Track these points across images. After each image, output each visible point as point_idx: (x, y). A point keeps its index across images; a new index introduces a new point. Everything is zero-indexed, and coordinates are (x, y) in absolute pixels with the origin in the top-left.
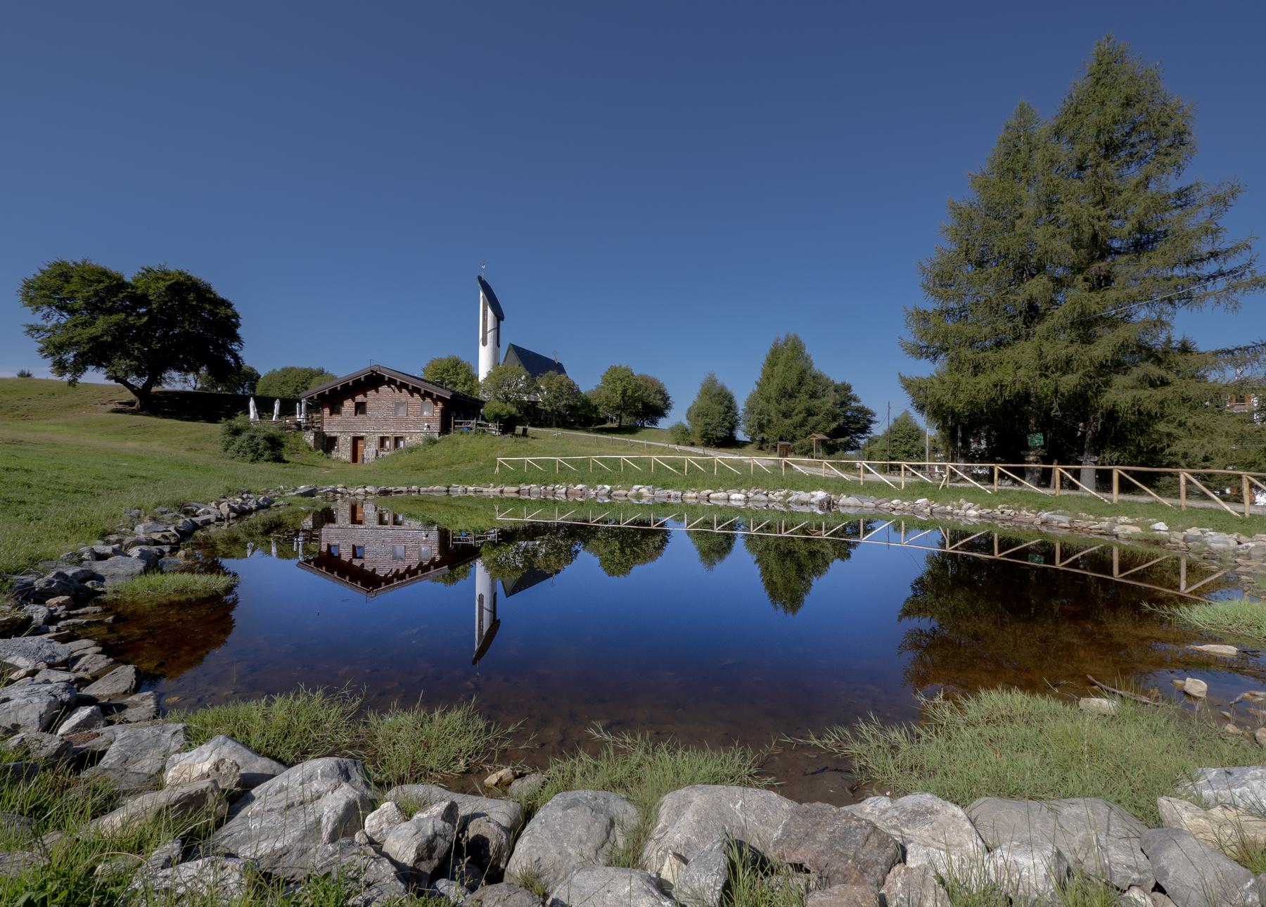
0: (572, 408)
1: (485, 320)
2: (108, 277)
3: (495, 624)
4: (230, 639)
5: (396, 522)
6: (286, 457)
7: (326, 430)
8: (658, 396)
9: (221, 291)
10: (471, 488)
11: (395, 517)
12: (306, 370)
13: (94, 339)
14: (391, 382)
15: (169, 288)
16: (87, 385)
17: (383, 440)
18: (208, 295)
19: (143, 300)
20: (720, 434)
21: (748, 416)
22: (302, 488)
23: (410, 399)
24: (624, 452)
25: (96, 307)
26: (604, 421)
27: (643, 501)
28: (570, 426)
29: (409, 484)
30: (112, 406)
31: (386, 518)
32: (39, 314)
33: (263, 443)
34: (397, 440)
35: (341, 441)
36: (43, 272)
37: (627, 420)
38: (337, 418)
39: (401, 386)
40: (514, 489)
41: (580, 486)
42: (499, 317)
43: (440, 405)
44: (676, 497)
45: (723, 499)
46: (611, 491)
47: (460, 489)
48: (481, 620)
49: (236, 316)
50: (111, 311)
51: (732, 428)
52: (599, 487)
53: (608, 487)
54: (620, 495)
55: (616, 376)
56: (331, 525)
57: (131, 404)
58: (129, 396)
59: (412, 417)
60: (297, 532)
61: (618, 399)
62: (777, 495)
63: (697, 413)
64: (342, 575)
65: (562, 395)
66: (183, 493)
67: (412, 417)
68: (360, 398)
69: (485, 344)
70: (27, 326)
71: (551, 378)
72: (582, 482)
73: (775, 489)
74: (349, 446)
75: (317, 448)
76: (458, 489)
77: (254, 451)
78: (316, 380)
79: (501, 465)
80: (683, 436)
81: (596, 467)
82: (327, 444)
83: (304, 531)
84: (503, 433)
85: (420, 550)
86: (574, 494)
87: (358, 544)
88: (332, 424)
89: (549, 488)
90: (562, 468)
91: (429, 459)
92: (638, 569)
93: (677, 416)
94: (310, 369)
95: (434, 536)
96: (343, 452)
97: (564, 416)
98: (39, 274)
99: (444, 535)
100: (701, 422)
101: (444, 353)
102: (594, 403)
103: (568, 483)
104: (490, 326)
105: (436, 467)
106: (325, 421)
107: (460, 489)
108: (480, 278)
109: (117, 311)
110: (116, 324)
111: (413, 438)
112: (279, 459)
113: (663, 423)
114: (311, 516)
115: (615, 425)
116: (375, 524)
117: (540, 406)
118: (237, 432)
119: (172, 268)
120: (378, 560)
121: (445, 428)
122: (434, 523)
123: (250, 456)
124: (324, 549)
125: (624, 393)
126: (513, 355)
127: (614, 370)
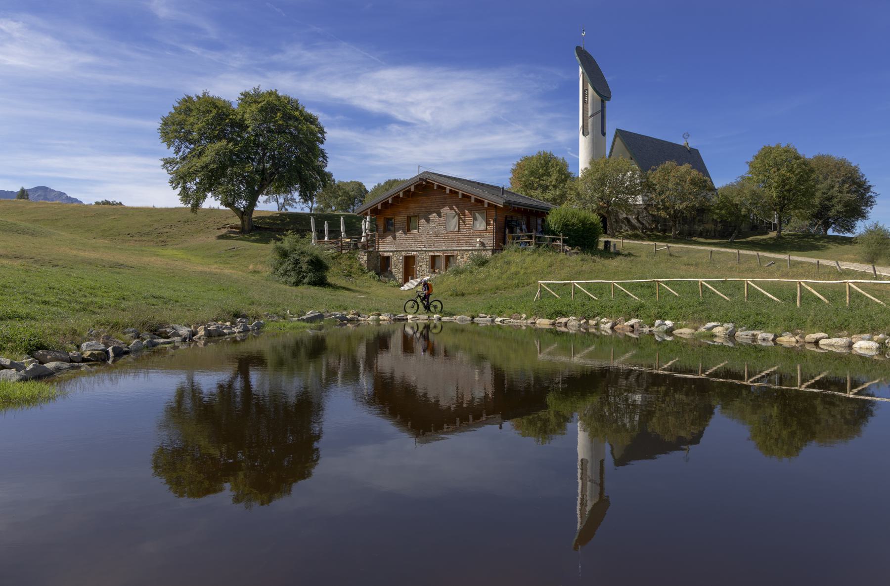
6: (330, 280)
15: (261, 110)
16: (212, 210)
17: (433, 258)
24: (751, 271)
28: (685, 237)
30: (223, 232)
35: (393, 261)
36: (175, 108)
41: (633, 321)
42: (604, 94)
52: (658, 322)
53: (669, 323)
55: (770, 161)
58: (237, 221)
70: (164, 160)
76: (484, 320)
89: (592, 322)
92: (812, 450)
95: (489, 376)
98: (173, 111)
99: (499, 376)
102: (736, 200)
112: (321, 282)
113: (860, 227)
121: (500, 244)
127: (767, 152)
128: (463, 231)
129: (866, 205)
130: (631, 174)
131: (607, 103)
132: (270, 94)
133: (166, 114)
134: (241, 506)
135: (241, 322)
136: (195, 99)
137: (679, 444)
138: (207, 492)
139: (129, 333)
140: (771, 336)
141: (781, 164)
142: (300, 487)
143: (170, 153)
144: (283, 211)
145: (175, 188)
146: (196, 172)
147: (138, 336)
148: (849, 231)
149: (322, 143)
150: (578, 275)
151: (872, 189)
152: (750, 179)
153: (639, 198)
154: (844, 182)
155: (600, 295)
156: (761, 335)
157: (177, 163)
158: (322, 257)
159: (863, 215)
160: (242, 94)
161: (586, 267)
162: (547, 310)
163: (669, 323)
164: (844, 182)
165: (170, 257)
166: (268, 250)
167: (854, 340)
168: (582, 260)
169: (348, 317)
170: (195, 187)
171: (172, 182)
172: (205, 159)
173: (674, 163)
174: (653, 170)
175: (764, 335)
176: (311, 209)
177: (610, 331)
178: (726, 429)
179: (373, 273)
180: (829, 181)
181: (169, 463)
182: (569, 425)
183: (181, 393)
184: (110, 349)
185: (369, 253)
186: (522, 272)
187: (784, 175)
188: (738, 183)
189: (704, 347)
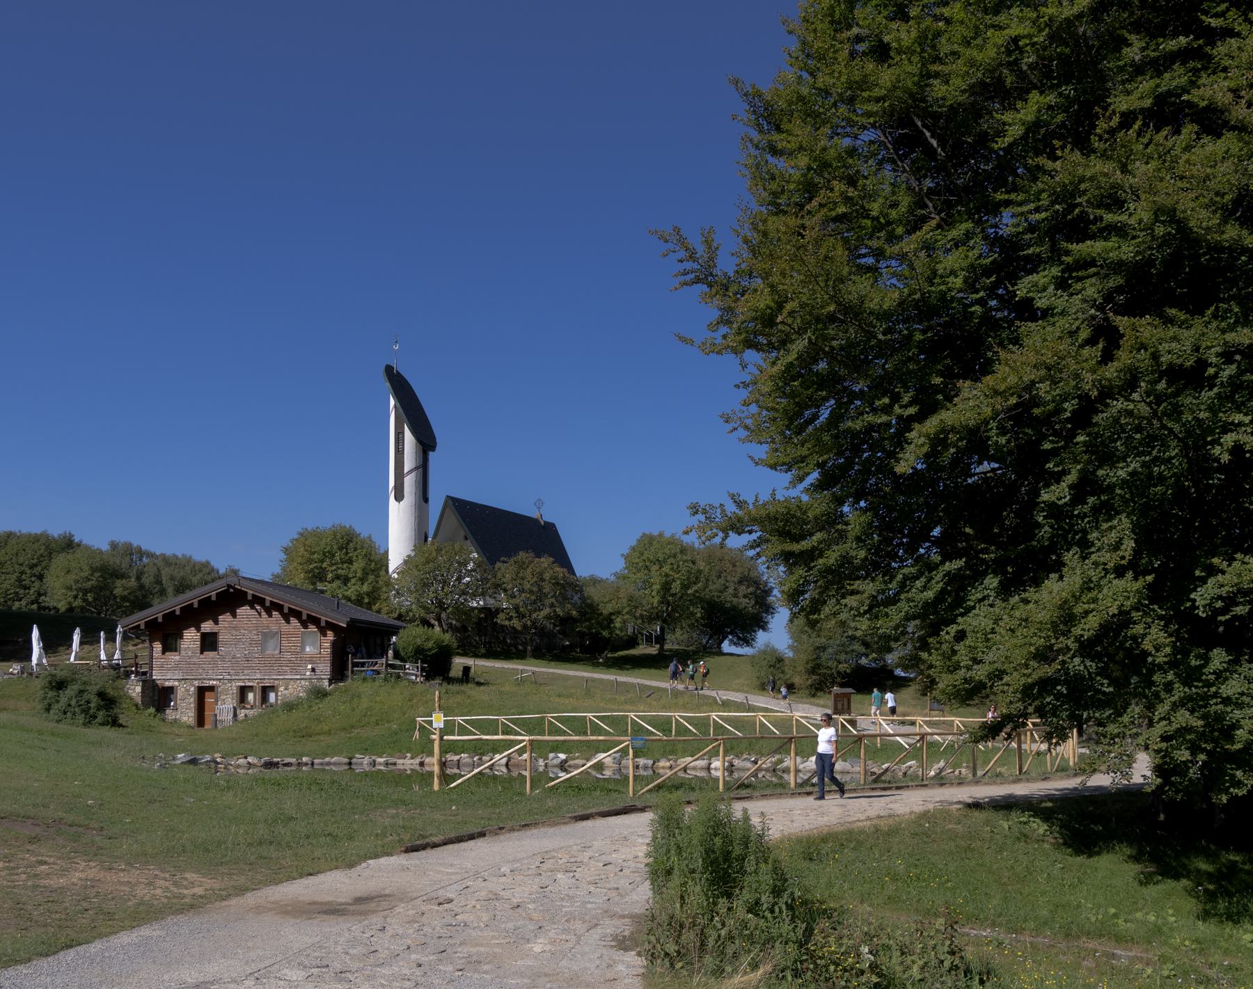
7: (156, 676)
8: (743, 589)
10: (381, 760)
12: (35, 539)
14: (257, 601)
17: (243, 691)
24: (676, 708)
26: (632, 642)
27: (608, 773)
33: (95, 702)
34: (265, 691)
35: (180, 693)
38: (173, 657)
42: (426, 443)
43: (331, 636)
44: (645, 768)
45: (702, 769)
46: (565, 761)
47: (366, 760)
52: (551, 755)
53: (562, 756)
59: (288, 656)
65: (541, 596)
67: (288, 656)
68: (207, 626)
69: (399, 498)
71: (522, 566)
74: (192, 701)
75: (146, 705)
77: (85, 711)
78: (60, 560)
84: (428, 678)
88: (168, 668)
91: (318, 720)
94: (45, 535)
101: (326, 517)
104: (408, 464)
105: (329, 733)
107: (366, 760)
108: (389, 369)
111: (291, 688)
112: (115, 723)
115: (653, 650)
117: (501, 619)
121: (339, 673)
123: (81, 718)
125: (666, 587)
126: (453, 520)
127: (648, 541)
129: (767, 612)
140: (650, 762)
141: (665, 561)
155: (666, 731)
163: (562, 756)
164: (740, 582)
177: (505, 770)
179: (152, 710)
180: (722, 581)
187: (667, 575)
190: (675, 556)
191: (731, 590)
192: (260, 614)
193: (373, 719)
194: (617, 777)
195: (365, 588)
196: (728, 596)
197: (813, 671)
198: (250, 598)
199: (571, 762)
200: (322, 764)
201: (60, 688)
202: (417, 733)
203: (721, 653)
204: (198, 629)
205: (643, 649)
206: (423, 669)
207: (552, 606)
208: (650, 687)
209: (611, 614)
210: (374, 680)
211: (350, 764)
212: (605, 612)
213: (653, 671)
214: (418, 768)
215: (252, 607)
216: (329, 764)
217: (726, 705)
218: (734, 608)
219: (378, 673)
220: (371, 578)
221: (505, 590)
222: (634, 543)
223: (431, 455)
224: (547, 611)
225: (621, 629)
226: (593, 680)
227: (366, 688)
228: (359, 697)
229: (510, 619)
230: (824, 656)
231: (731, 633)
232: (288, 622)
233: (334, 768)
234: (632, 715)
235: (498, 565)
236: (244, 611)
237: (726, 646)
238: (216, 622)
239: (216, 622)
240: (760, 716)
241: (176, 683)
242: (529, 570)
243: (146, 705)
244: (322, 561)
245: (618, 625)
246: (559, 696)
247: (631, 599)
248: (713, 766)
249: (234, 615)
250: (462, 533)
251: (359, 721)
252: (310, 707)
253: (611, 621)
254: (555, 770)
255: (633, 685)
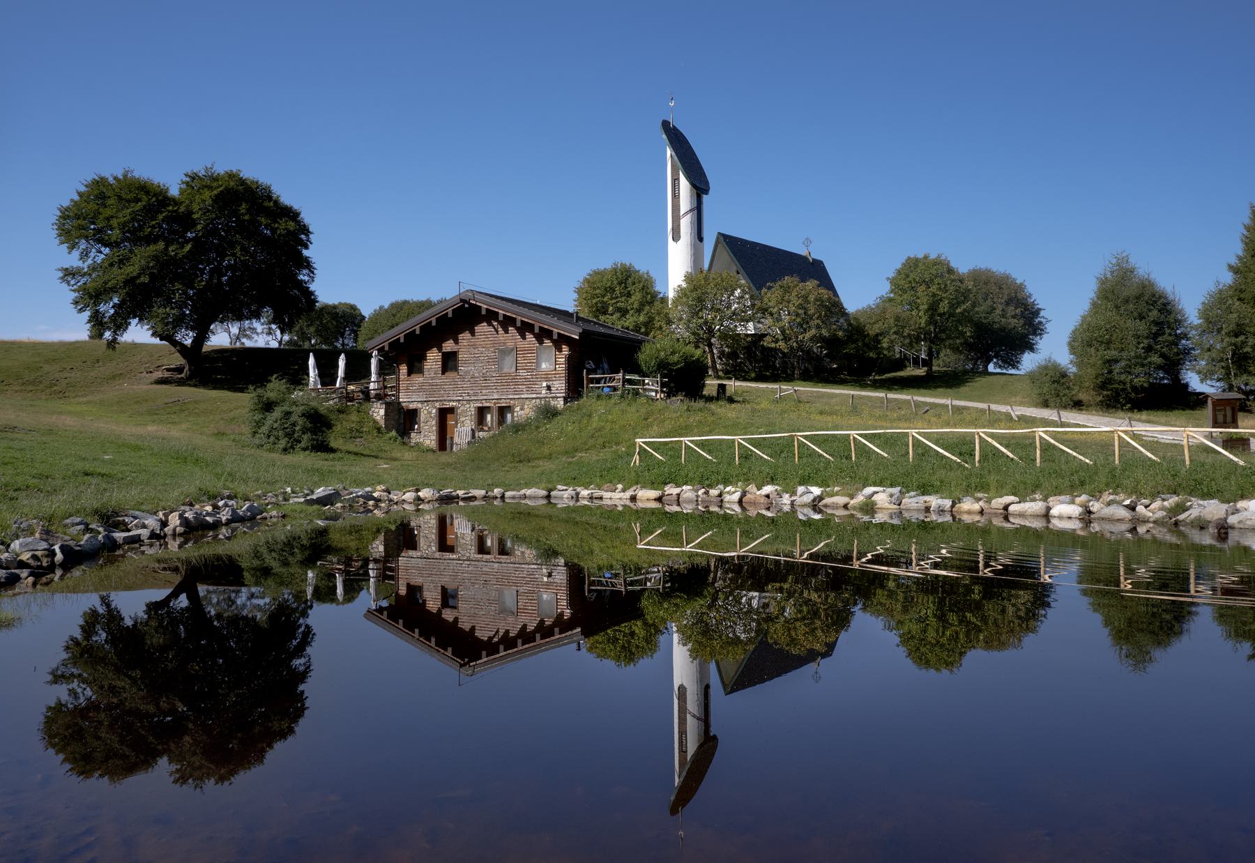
0: (832, 343)
1: (676, 196)
2: (147, 193)
3: (708, 742)
4: (302, 726)
5: (503, 551)
8: (1011, 310)
9: (287, 198)
10: (585, 493)
11: (501, 543)
13: (130, 281)
14: (491, 316)
15: (216, 199)
16: (135, 346)
17: (482, 412)
18: (266, 204)
19: (186, 220)
20: (1140, 381)
21: (1210, 340)
22: (320, 492)
23: (521, 344)
24: (908, 420)
25: (135, 236)
26: (900, 364)
27: (880, 518)
29: (490, 487)
30: (158, 375)
31: (489, 543)
32: (76, 254)
34: (503, 411)
35: (423, 416)
36: (80, 194)
37: (946, 360)
38: (418, 379)
39: (507, 322)
40: (654, 494)
41: (768, 489)
42: (700, 187)
44: (941, 511)
46: (820, 498)
48: (683, 732)
49: (305, 230)
50: (150, 240)
51: (1173, 365)
52: (801, 489)
53: (816, 491)
54: (835, 506)
55: (919, 277)
56: (411, 553)
57: (179, 370)
58: (178, 360)
60: (366, 561)
61: (921, 319)
62: (1153, 510)
63: (1084, 341)
64: (426, 635)
66: (116, 497)
67: (522, 373)
68: (449, 346)
71: (787, 290)
72: (772, 481)
73: (1154, 496)
75: (388, 429)
76: (564, 495)
77: (289, 435)
79: (643, 452)
80: (1056, 390)
81: (805, 453)
82: (404, 420)
83: (376, 561)
85: (539, 599)
86: (754, 504)
87: (450, 586)
88: (414, 391)
89: (714, 492)
90: (746, 456)
91: (541, 443)
92: (977, 659)
93: (1053, 348)
95: (561, 576)
96: (426, 435)
97: (819, 359)
99: (576, 576)
100: (1097, 356)
101: (606, 258)
102: (873, 330)
103: (747, 481)
104: (685, 203)
106: (403, 385)
108: (665, 124)
109: (155, 241)
110: (155, 258)
112: (322, 447)
113: (1029, 362)
114: (381, 537)
115: (921, 372)
116: (472, 552)
118: (268, 406)
119: (221, 169)
120: (477, 615)
121: (575, 389)
122: (556, 554)
124: (403, 591)
125: (933, 308)
127: (912, 264)
128: (522, 373)
129: (1035, 334)
130: (739, 297)
131: (705, 197)
132: (231, 176)
133: (66, 203)
134: (188, 788)
135: (226, 505)
136: (111, 180)
137: (812, 656)
138: (131, 768)
139: (74, 525)
140: (947, 503)
141: (932, 281)
142: (279, 751)
143: (73, 260)
144: (238, 345)
145: (81, 311)
146: (114, 290)
147: (87, 529)
148: (1014, 367)
149: (307, 247)
150: (685, 430)
151: (1042, 313)
152: (890, 300)
153: (751, 325)
154: (1007, 304)
156: (934, 501)
157: (83, 275)
158: (322, 410)
159: (1031, 348)
160: (186, 175)
161: (694, 419)
162: (666, 479)
163: (816, 491)
164: (1007, 304)
165: (76, 419)
166: (242, 402)
167: (1051, 504)
168: (688, 410)
169: (375, 495)
170: (112, 311)
171: (76, 303)
172: (132, 269)
173: (796, 279)
174: (770, 288)
175: (940, 501)
176: (280, 343)
177: (737, 509)
178: (870, 637)
180: (989, 302)
181: (71, 733)
182: (662, 639)
183: (91, 621)
184: (57, 548)
185: (388, 405)
186: (608, 426)
187: (934, 295)
188: (878, 306)
189: (861, 526)
190: (942, 276)
191: (998, 312)
192: (497, 331)
193: (601, 441)
194: (896, 521)
195: (642, 318)
196: (996, 316)
197: (1103, 386)
198: (484, 312)
199: (828, 501)
200: (513, 498)
201: (268, 411)
202: (637, 457)
203: (986, 373)
204: (440, 349)
205: (911, 371)
206: (663, 385)
207: (818, 327)
208: (926, 404)
209: (877, 335)
210: (610, 397)
211: (548, 497)
212: (872, 333)
213: (923, 391)
214: (628, 503)
215: (490, 324)
216: (525, 497)
217: (995, 420)
218: (1003, 329)
219: (615, 389)
220: (647, 308)
221: (771, 314)
222: (899, 266)
223: (705, 198)
224: (813, 332)
225: (888, 349)
226: (861, 397)
227: (600, 407)
228: (590, 416)
229: (777, 341)
230: (1117, 368)
231: (996, 357)
232: (524, 338)
233: (529, 502)
234: (914, 432)
235: (764, 290)
236: (482, 328)
237: (991, 368)
238: (456, 342)
239: (456, 342)
240: (1040, 432)
241: (420, 405)
242: (794, 294)
243: (388, 429)
244: (603, 296)
245: (885, 345)
246: (821, 413)
247: (897, 319)
248: (1054, 512)
249: (473, 334)
250: (735, 268)
251: (585, 443)
252: (537, 428)
253: (879, 342)
254: (806, 510)
255: (908, 402)
